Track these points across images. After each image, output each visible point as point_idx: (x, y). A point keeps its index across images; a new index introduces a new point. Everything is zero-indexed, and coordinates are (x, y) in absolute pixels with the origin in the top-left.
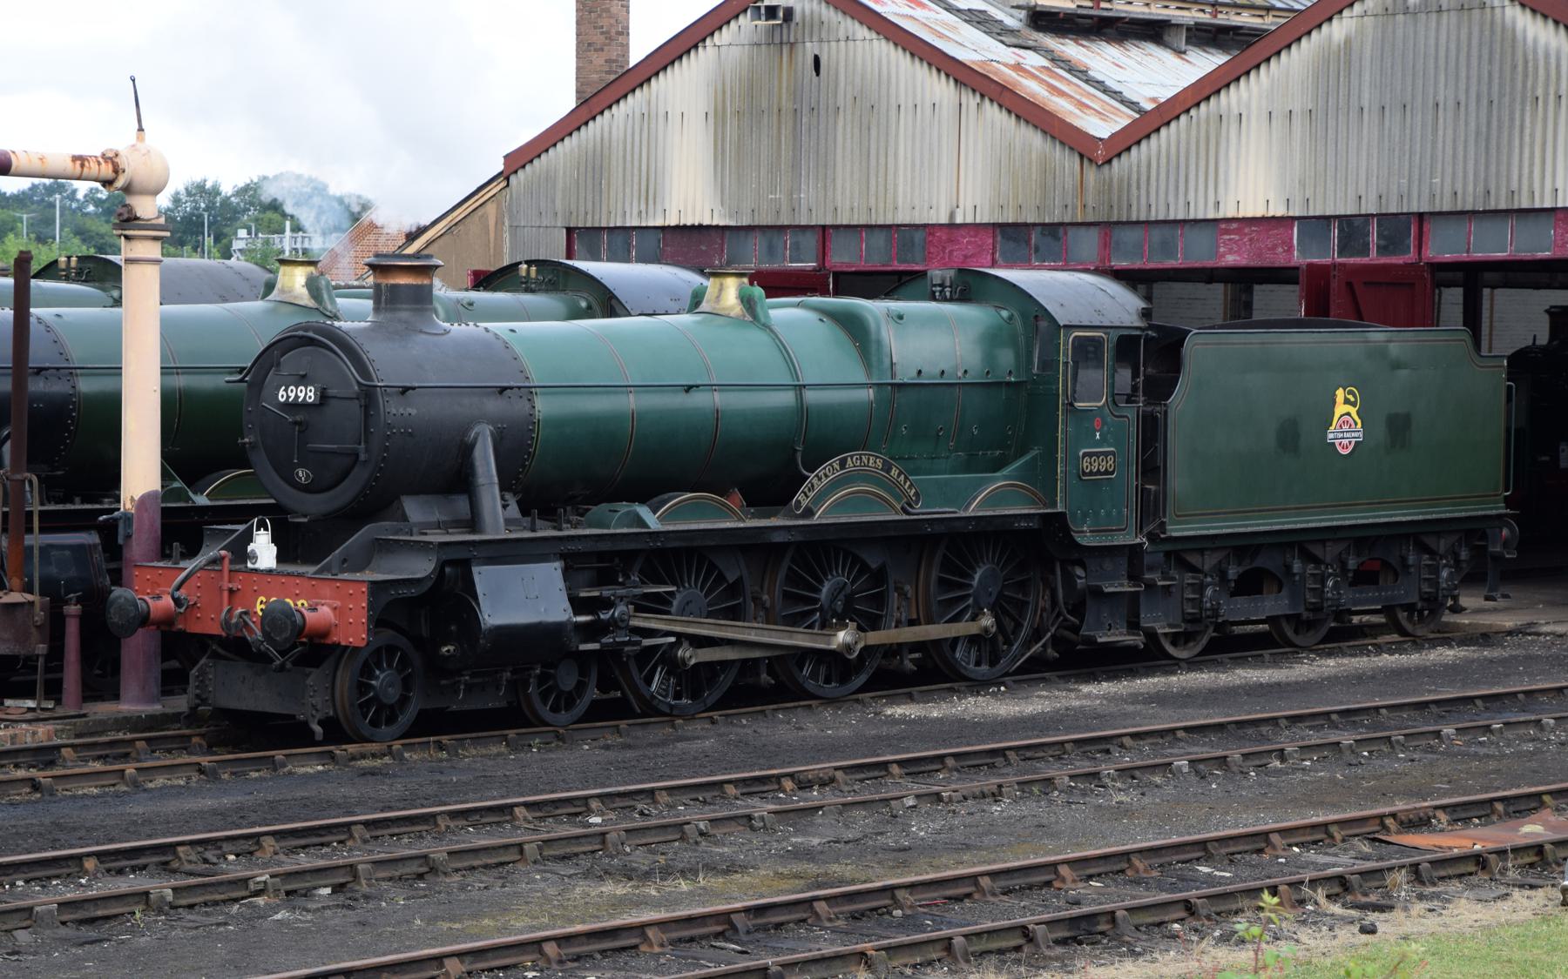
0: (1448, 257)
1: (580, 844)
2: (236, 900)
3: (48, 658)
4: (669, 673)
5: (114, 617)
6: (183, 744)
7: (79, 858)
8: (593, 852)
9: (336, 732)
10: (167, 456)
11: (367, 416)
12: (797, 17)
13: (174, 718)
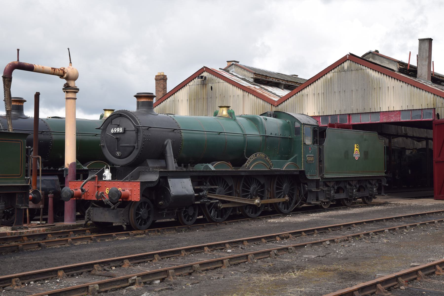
0: (356, 123)
1: (240, 260)
2: (124, 288)
3: (43, 209)
4: (215, 211)
5: (63, 195)
6: (83, 232)
7: (56, 271)
8: (244, 262)
9: (130, 228)
10: (77, 158)
11: (137, 136)
12: (207, 79)
13: (81, 226)
